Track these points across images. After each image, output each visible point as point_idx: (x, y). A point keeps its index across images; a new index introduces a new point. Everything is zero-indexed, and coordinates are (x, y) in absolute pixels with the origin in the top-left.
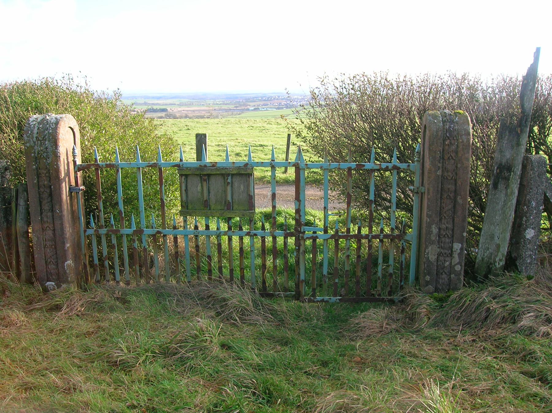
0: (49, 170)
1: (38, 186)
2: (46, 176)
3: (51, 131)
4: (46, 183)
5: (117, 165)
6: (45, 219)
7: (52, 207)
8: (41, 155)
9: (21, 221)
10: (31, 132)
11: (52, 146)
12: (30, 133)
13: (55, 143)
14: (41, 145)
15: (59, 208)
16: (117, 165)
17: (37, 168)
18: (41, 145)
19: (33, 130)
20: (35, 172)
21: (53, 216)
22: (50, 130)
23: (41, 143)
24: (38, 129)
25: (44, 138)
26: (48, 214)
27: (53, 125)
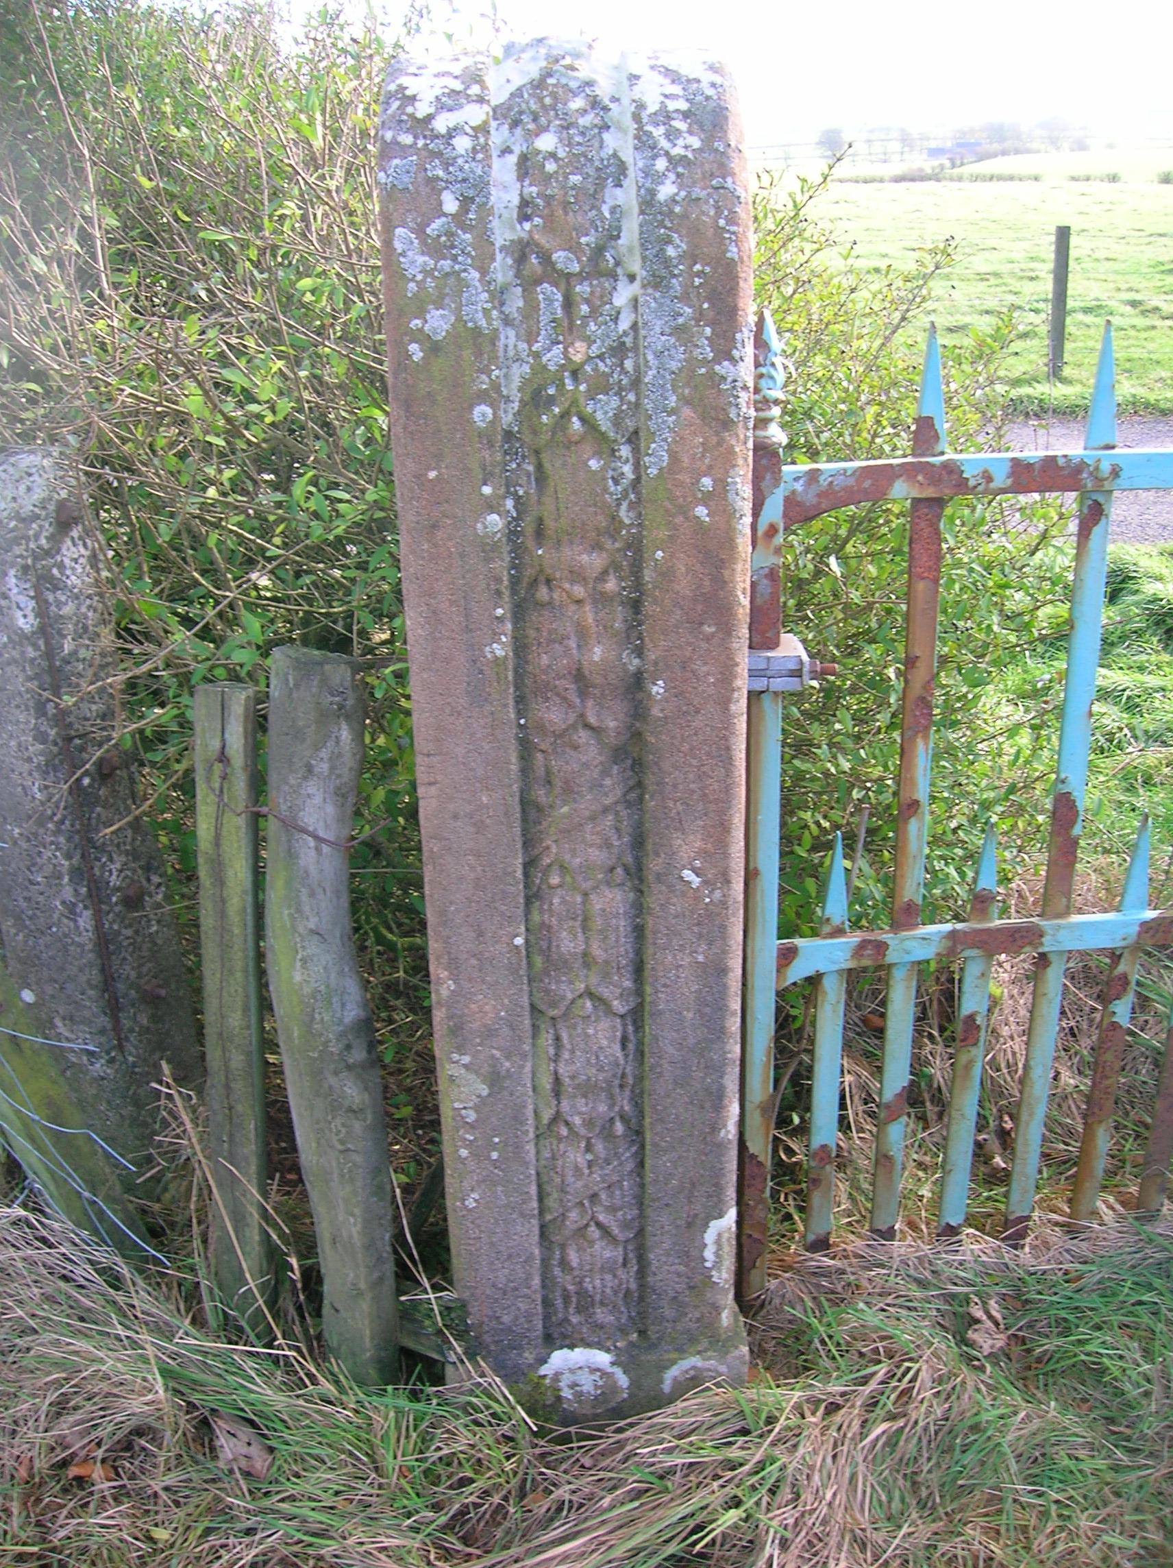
0: (636, 547)
1: (519, 684)
2: (601, 599)
3: (666, 190)
4: (597, 653)
5: (1105, 467)
6: (568, 943)
7: (639, 842)
8: (565, 415)
9: (313, 947)
10: (466, 202)
11: (678, 331)
12: (450, 204)
13: (713, 297)
14: (568, 327)
15: (703, 854)
16: (1105, 467)
17: (513, 534)
18: (568, 327)
19: (482, 185)
20: (501, 566)
21: (638, 909)
22: (660, 178)
23: (568, 304)
24: (526, 166)
25: (599, 250)
26: (597, 903)
27: (672, 135)
